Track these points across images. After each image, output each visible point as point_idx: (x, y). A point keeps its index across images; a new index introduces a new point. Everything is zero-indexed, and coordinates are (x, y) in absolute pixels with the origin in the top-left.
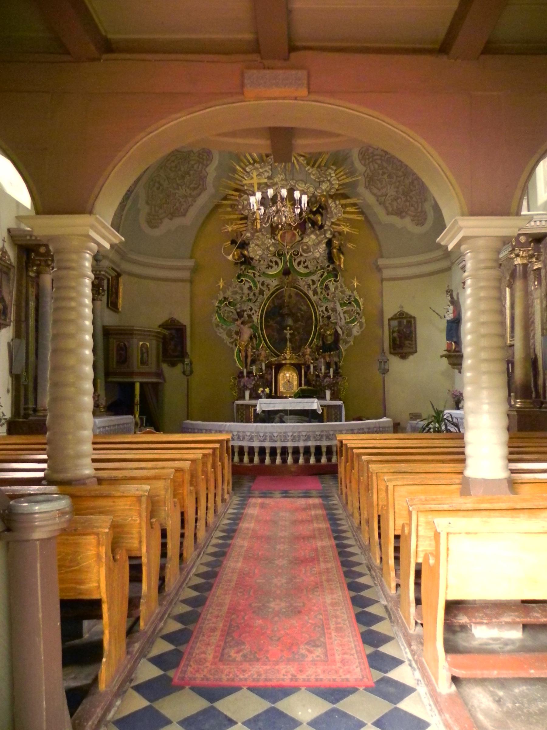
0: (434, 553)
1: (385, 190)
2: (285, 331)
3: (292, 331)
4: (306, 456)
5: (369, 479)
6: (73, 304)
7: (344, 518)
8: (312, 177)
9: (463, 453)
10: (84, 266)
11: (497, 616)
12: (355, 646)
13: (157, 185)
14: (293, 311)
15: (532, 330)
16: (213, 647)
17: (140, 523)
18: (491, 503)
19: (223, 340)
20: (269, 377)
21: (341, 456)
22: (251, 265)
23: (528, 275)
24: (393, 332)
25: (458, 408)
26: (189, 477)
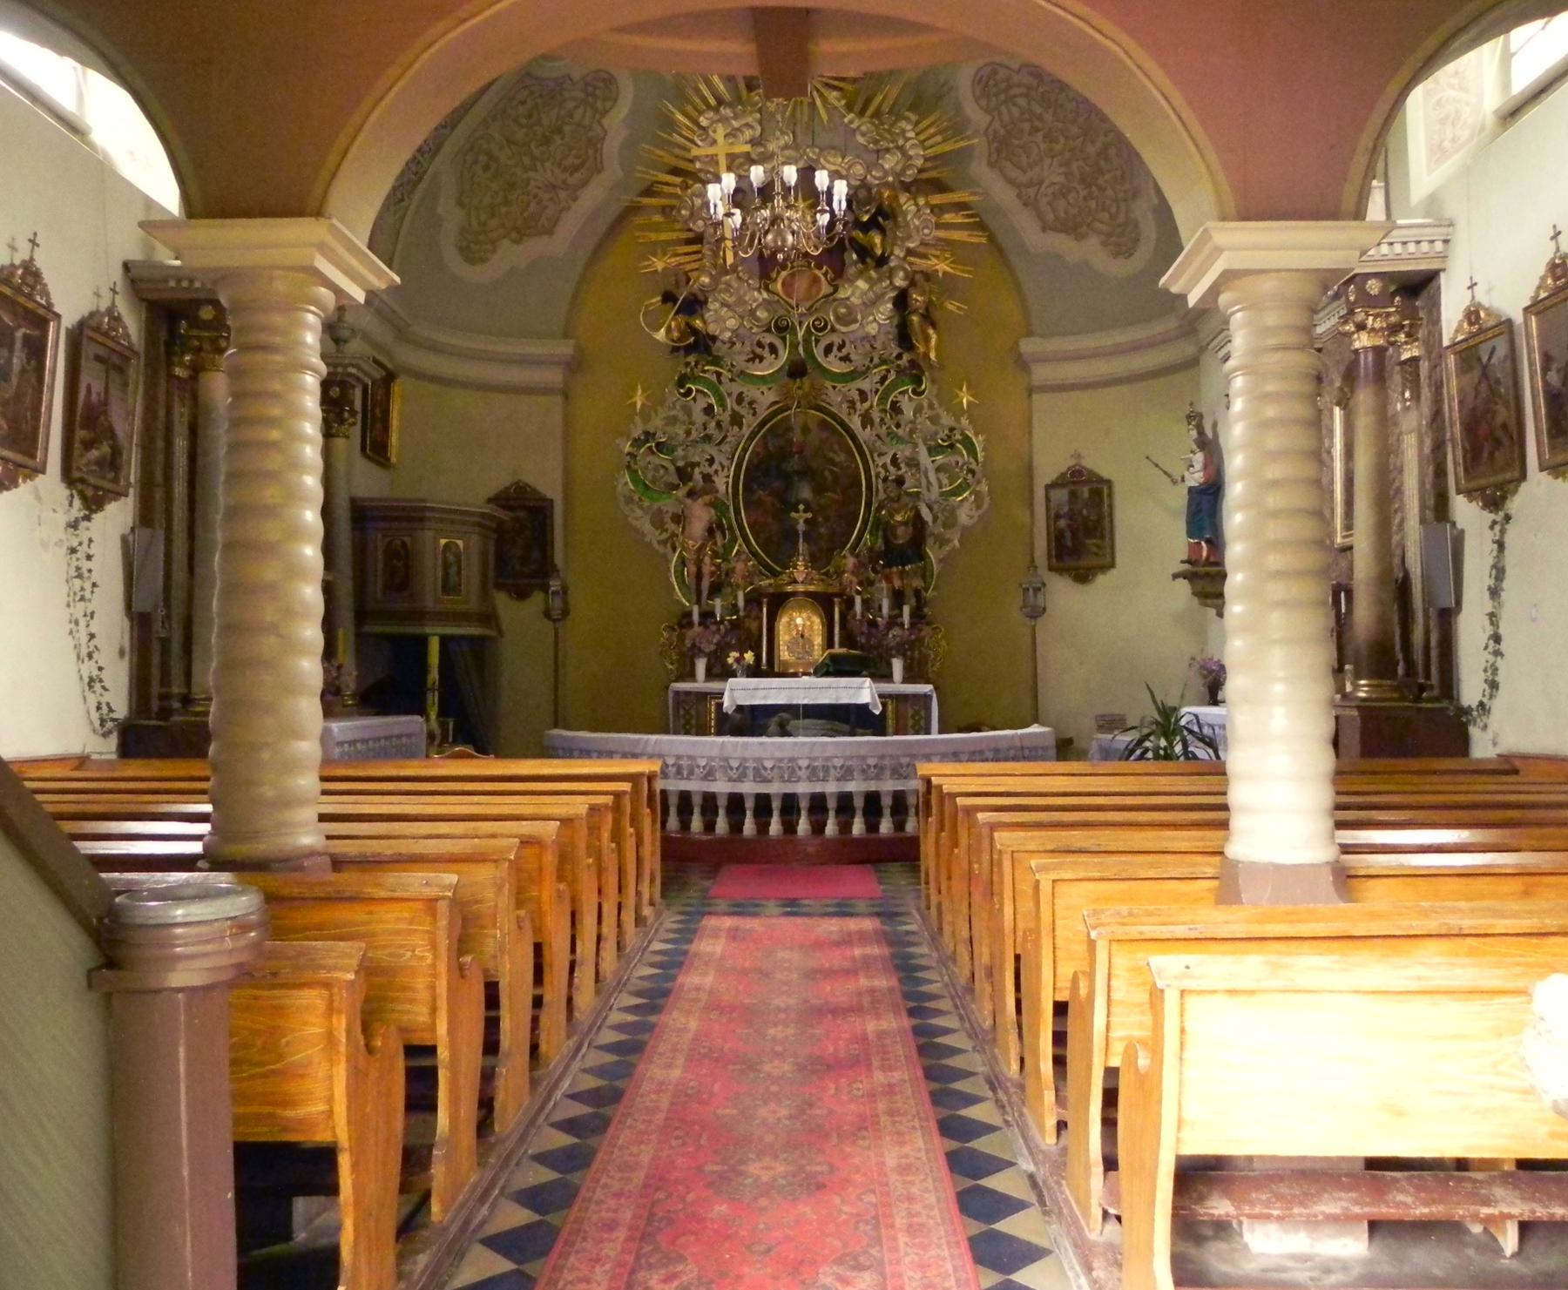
0: (1150, 1043)
1: (1037, 169)
2: (793, 514)
3: (809, 515)
4: (842, 819)
5: (995, 870)
6: (275, 435)
7: (934, 965)
8: (860, 139)
9: (1225, 808)
10: (304, 344)
11: (1306, 1199)
12: (955, 1269)
13: (483, 159)
14: (814, 465)
15: (1396, 511)
16: (607, 1267)
17: (434, 966)
18: (1291, 922)
19: (643, 534)
20: (754, 626)
21: (928, 814)
22: (710, 354)
23: (1387, 375)
24: (1058, 517)
25: (1214, 700)
26: (556, 861)
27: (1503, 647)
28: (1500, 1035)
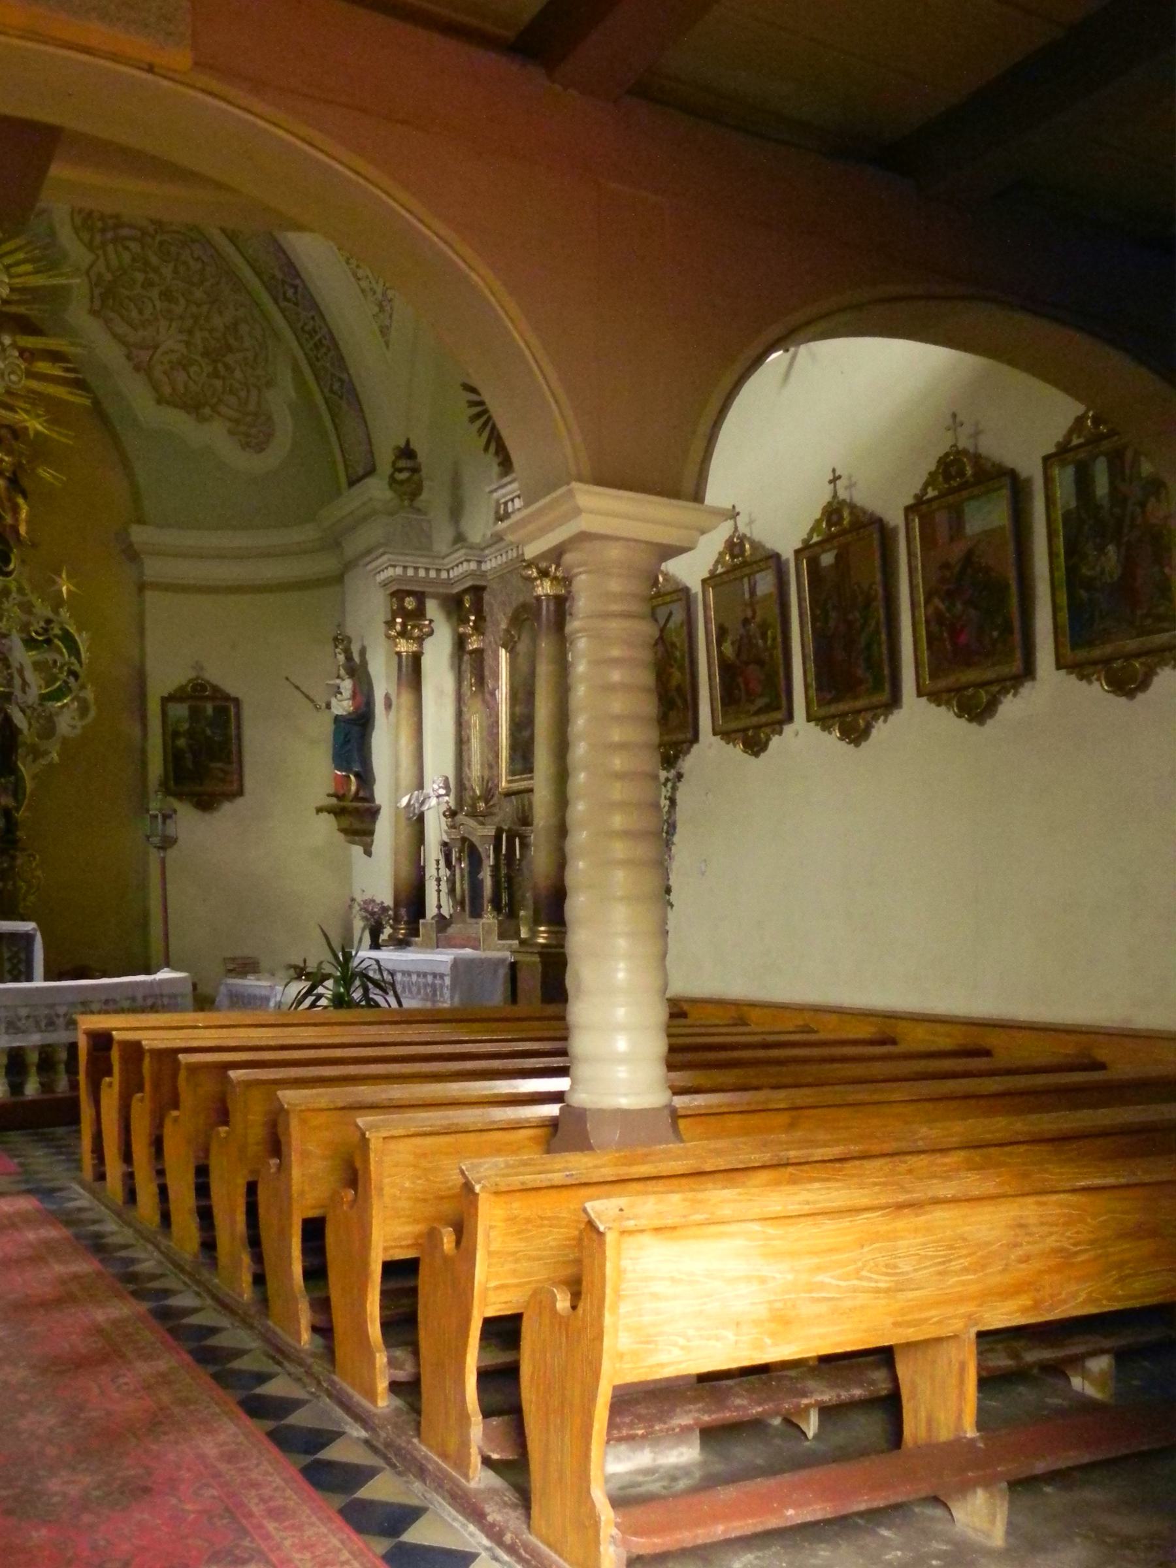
11: (662, 1417)
12: (342, 1541)
27: (673, 897)
28: (862, 1246)
